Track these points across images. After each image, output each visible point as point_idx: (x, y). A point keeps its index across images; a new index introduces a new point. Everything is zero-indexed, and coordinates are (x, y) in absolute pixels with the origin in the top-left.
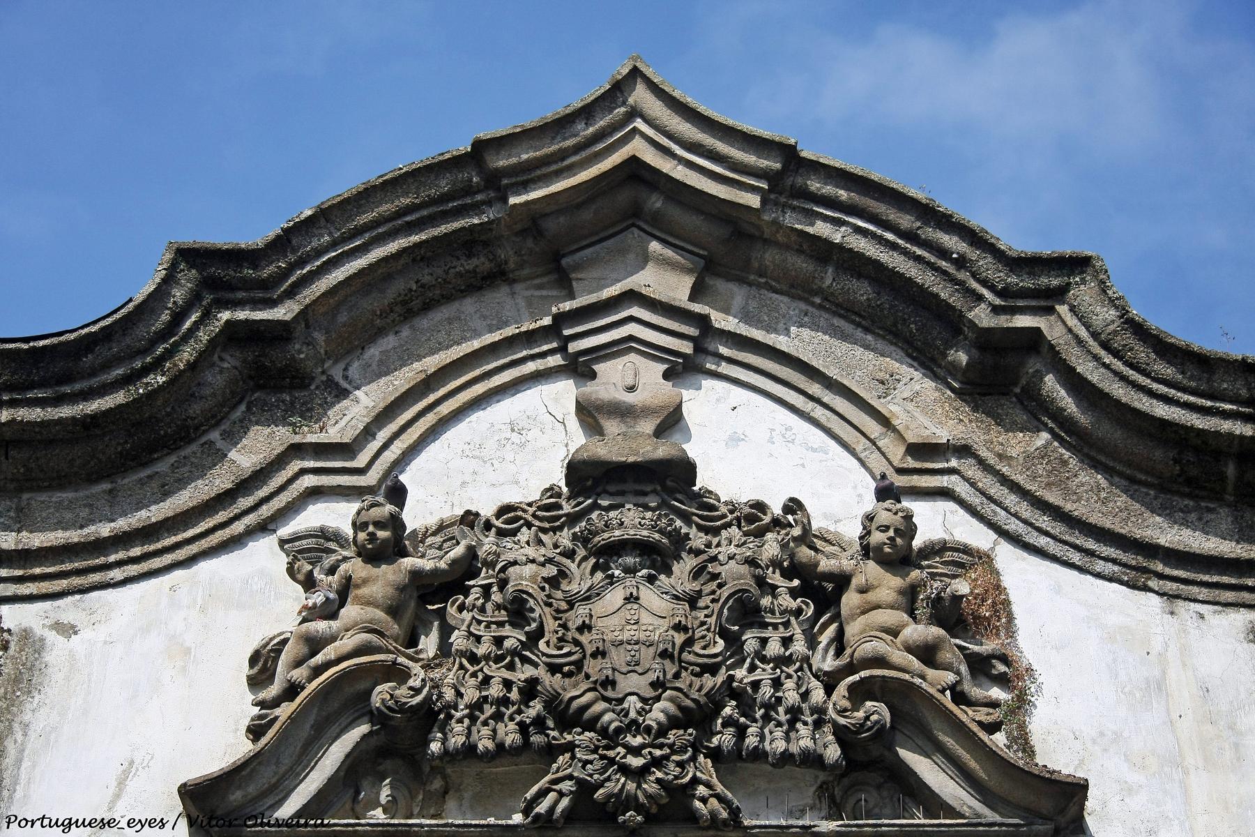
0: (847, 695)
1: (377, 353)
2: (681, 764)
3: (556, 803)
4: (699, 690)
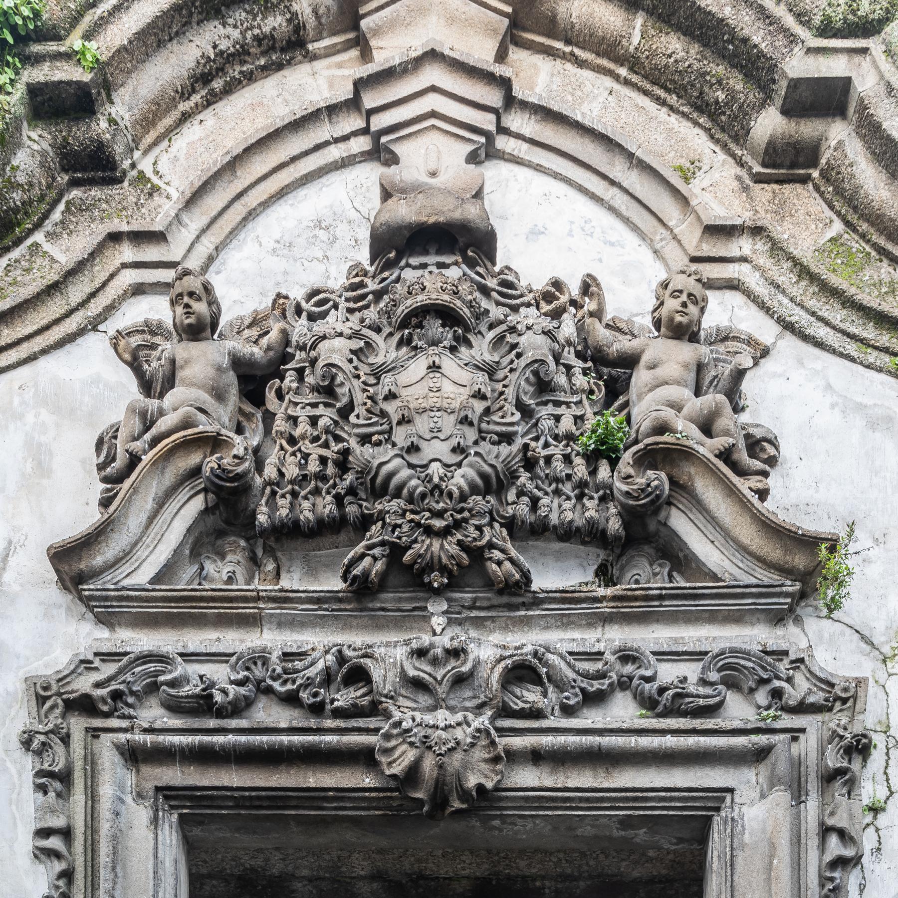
0: (631, 463)
1: (184, 145)
2: (479, 528)
3: (372, 566)
4: (497, 457)
